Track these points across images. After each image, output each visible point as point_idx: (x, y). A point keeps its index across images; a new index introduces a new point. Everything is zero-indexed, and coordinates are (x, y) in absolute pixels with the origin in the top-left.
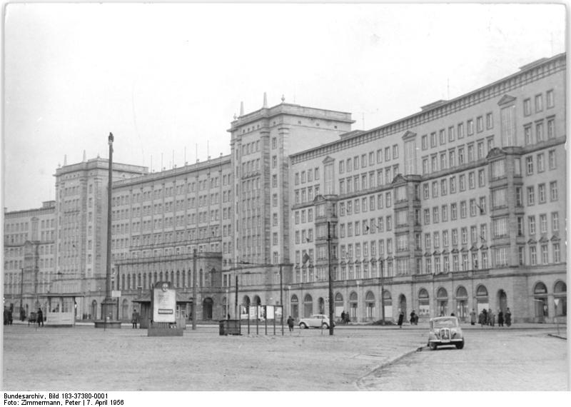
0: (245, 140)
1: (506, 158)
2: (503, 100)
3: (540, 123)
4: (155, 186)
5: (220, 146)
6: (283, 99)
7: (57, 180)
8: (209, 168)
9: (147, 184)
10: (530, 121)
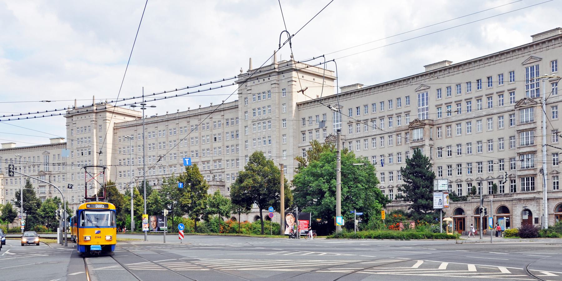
5: (230, 94)
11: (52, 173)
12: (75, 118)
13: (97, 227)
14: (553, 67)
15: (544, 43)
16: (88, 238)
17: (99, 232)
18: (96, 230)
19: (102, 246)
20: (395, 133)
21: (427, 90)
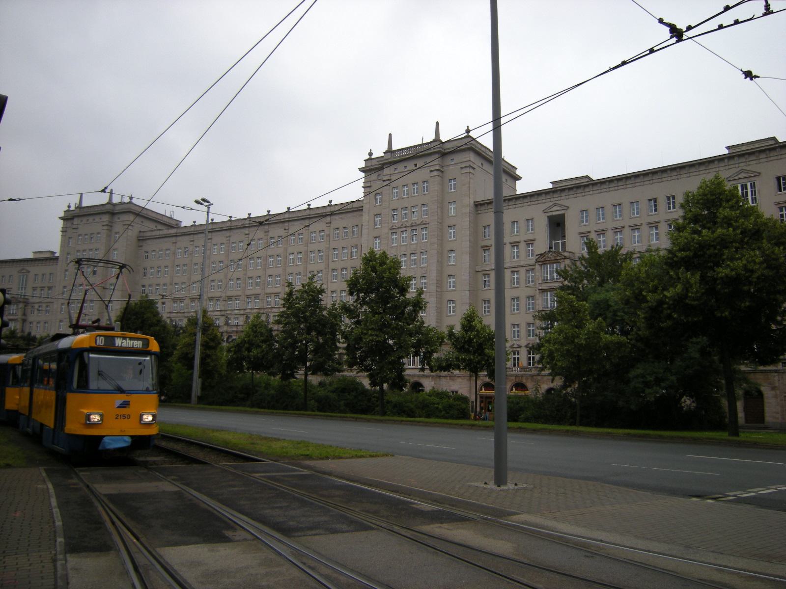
12: (76, 221)
13: (121, 391)
14: (669, 203)
15: (763, 151)
16: (95, 418)
17: (125, 404)
18: (120, 399)
19: (132, 437)
20: (253, 296)
21: (752, 179)
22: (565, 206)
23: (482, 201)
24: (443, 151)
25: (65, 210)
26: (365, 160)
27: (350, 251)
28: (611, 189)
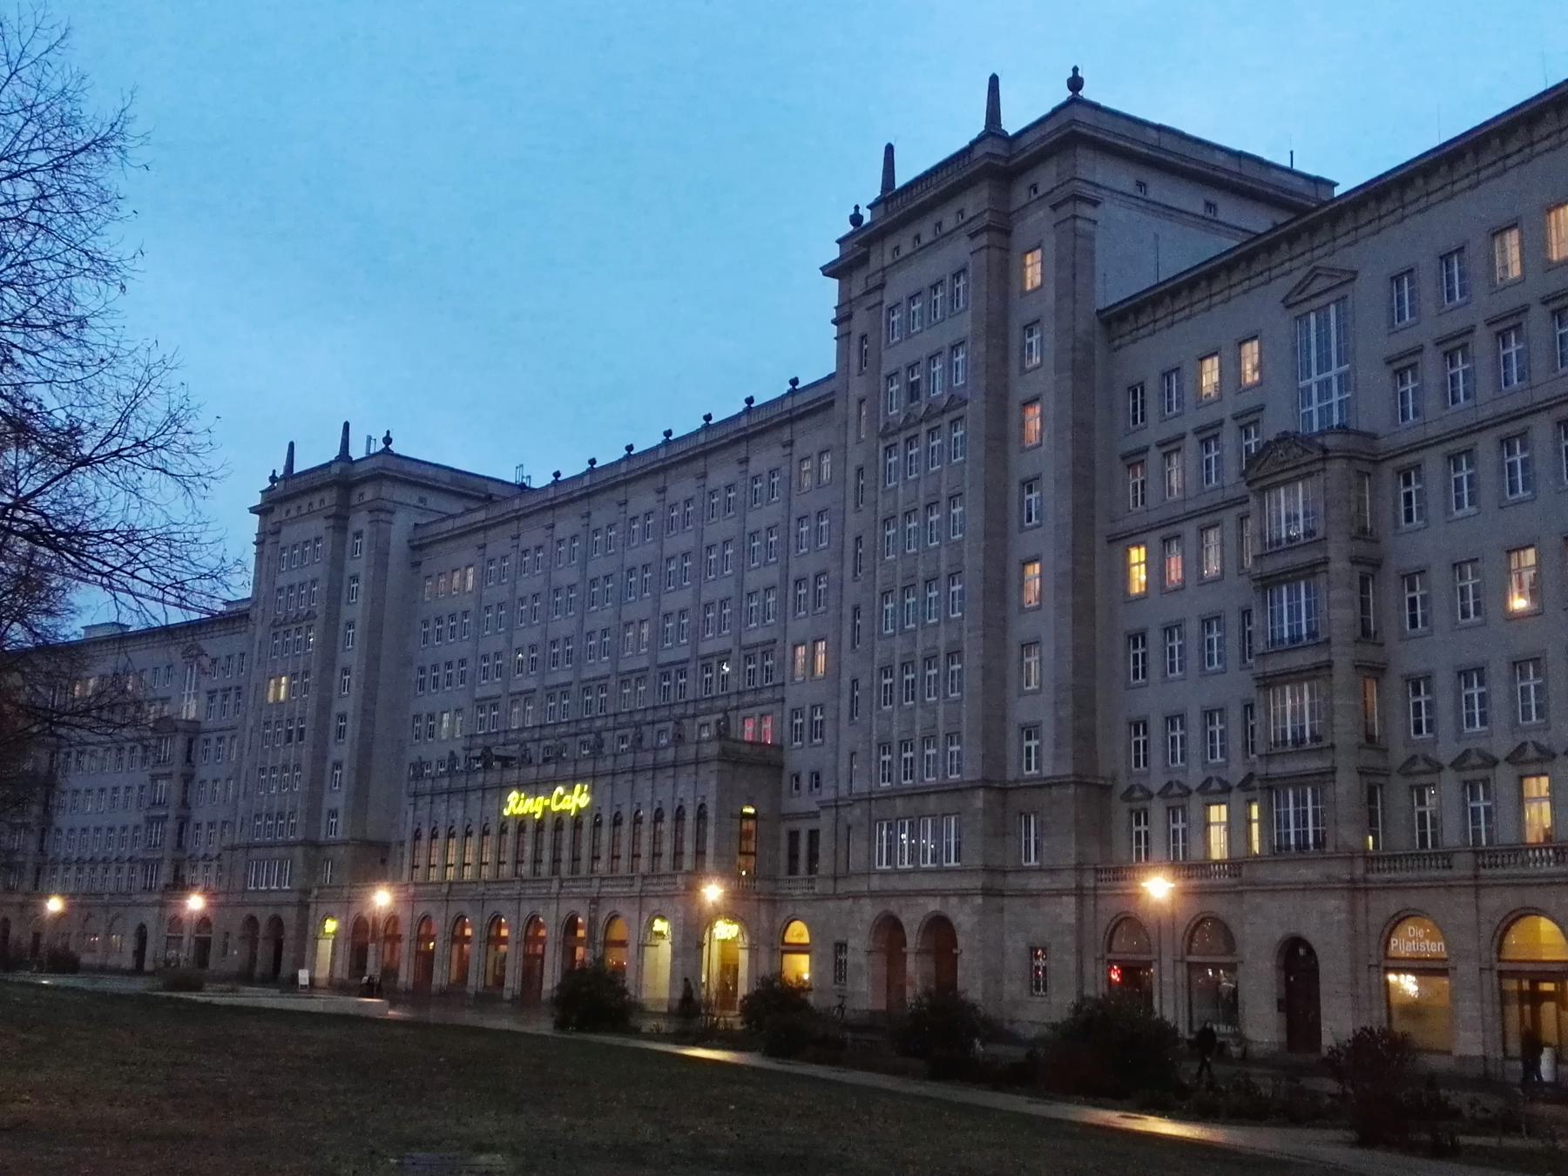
0: (290, 534)
1: (1324, 470)
2: (1301, 287)
3: (1210, 433)
4: (671, 489)
6: (1075, 83)
7: (262, 525)
8: (518, 518)
9: (533, 520)
10: (1180, 430)
11: (1383, 444)
22: (1343, 271)
23: (1211, 260)
24: (1002, 164)
25: (841, 235)
26: (839, 242)
27: (814, 525)
28: (1484, 174)
